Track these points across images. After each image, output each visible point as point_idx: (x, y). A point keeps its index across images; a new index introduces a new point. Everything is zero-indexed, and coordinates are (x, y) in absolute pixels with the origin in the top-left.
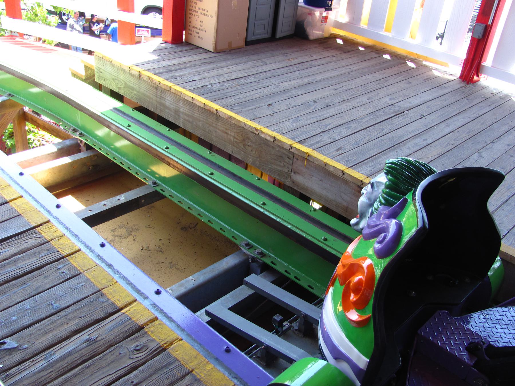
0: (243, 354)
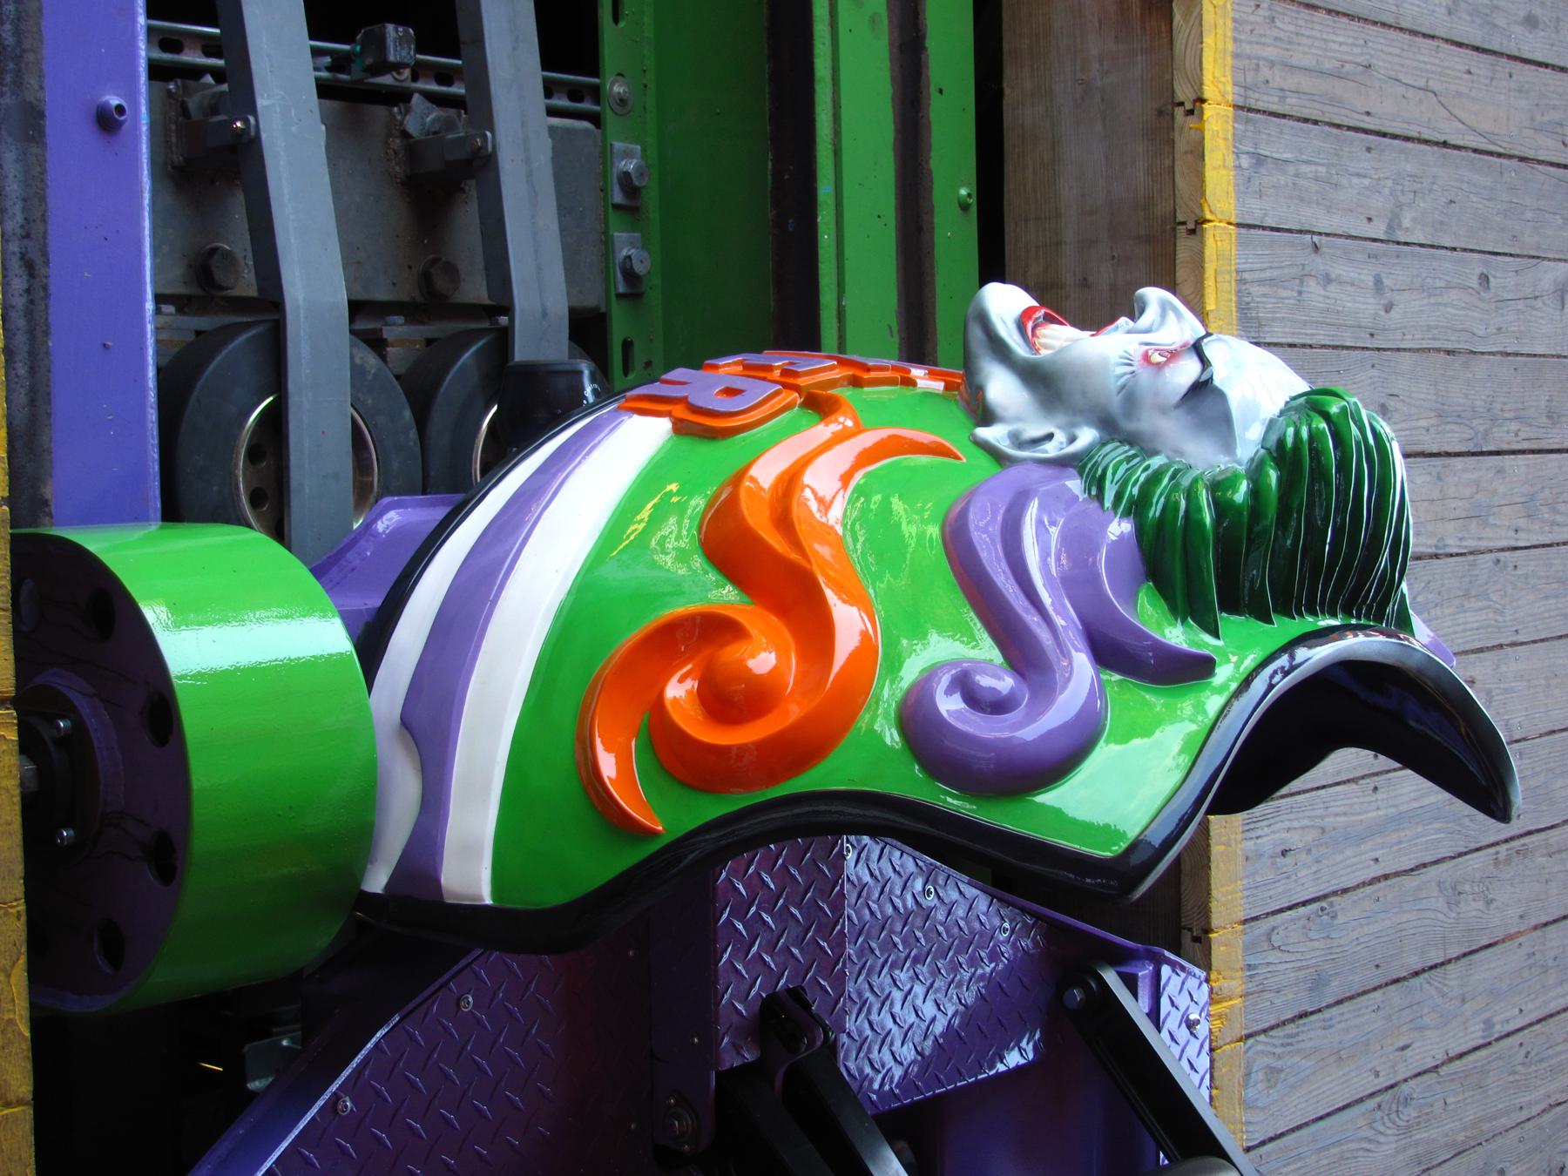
0: (142, 20)
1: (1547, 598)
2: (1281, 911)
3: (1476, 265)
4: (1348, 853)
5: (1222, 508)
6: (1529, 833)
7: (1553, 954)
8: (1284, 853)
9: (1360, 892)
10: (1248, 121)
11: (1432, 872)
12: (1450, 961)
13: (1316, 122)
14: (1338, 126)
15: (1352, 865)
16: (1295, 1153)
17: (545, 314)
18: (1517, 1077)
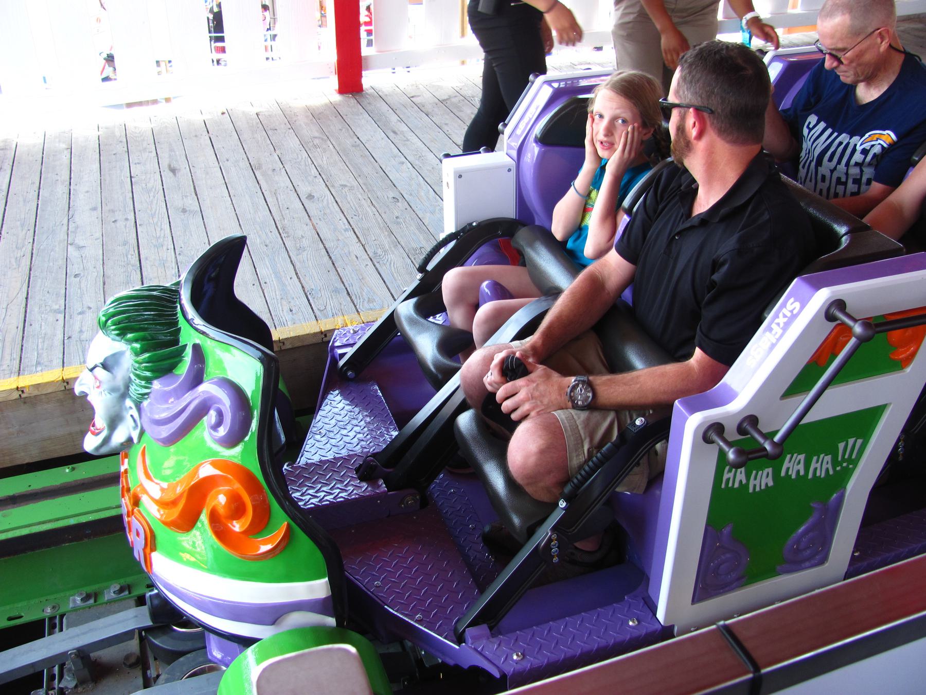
1: (191, 235)
2: (312, 308)
3: (71, 279)
4: (289, 288)
5: (143, 351)
6: (277, 227)
7: (319, 212)
8: (291, 311)
9: (303, 282)
10: (24, 370)
11: (293, 258)
12: (325, 247)
13: (22, 346)
14: (23, 337)
15: (294, 287)
16: (397, 288)
17: (136, 616)
18: (363, 217)
